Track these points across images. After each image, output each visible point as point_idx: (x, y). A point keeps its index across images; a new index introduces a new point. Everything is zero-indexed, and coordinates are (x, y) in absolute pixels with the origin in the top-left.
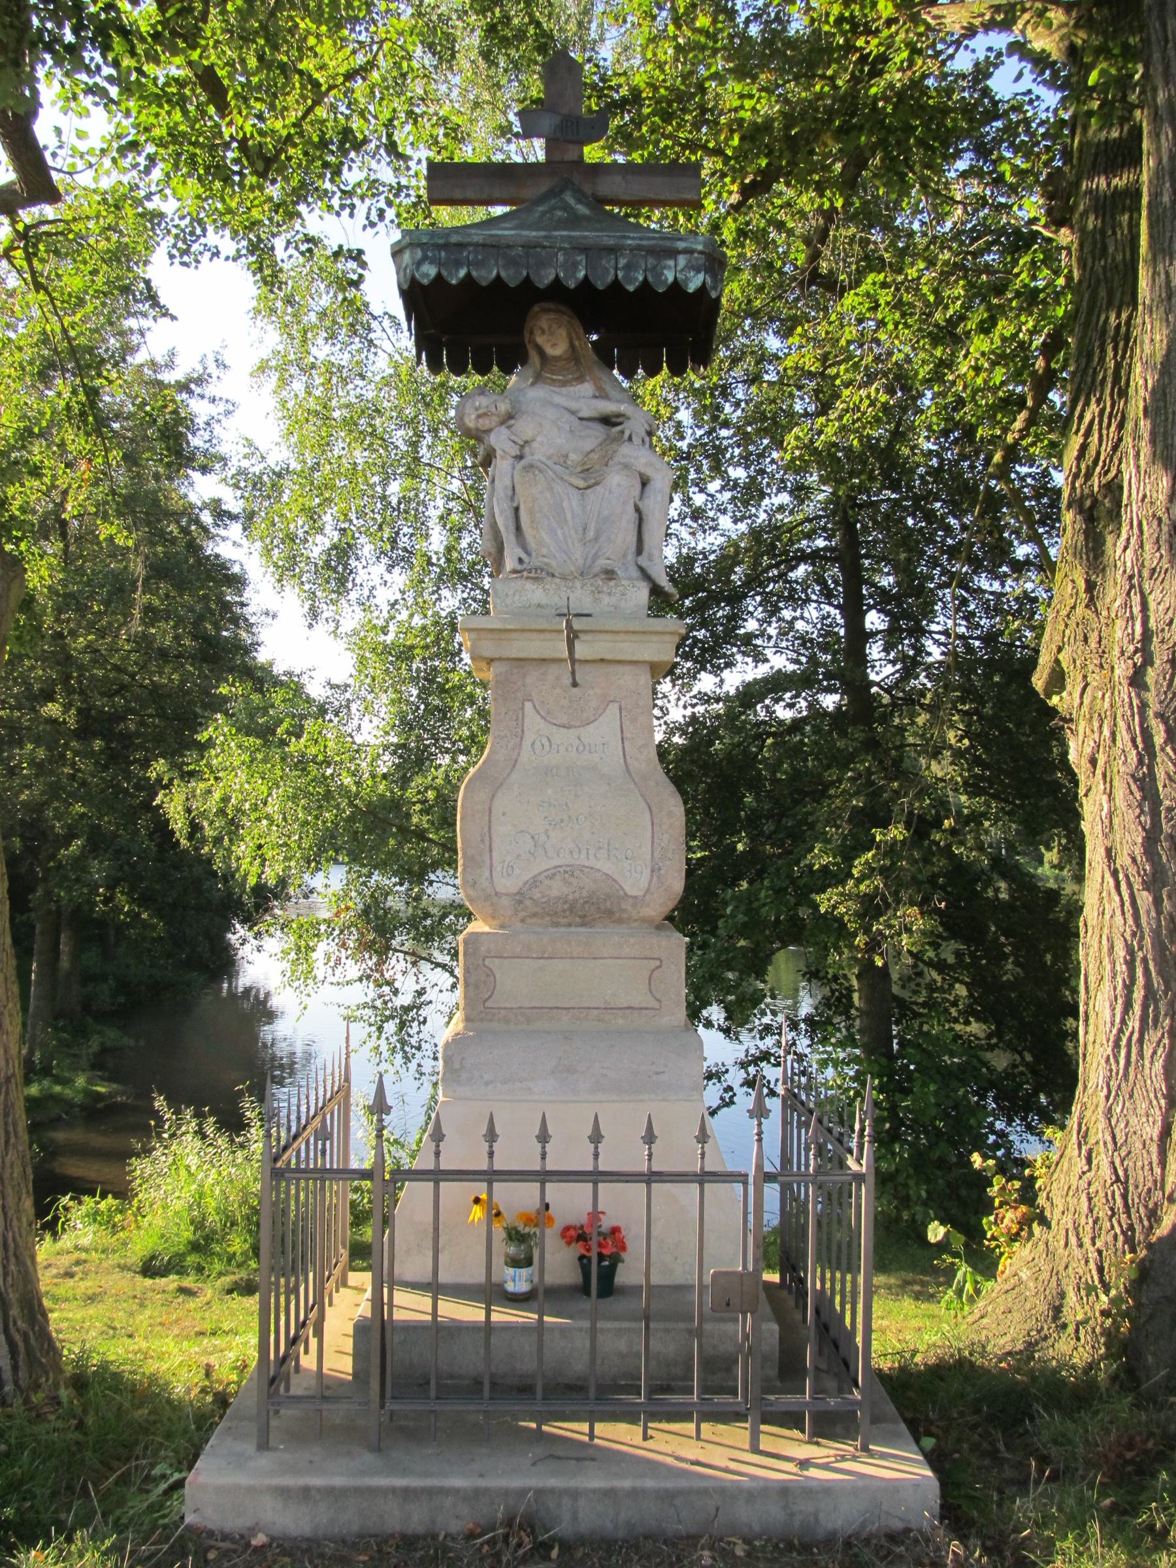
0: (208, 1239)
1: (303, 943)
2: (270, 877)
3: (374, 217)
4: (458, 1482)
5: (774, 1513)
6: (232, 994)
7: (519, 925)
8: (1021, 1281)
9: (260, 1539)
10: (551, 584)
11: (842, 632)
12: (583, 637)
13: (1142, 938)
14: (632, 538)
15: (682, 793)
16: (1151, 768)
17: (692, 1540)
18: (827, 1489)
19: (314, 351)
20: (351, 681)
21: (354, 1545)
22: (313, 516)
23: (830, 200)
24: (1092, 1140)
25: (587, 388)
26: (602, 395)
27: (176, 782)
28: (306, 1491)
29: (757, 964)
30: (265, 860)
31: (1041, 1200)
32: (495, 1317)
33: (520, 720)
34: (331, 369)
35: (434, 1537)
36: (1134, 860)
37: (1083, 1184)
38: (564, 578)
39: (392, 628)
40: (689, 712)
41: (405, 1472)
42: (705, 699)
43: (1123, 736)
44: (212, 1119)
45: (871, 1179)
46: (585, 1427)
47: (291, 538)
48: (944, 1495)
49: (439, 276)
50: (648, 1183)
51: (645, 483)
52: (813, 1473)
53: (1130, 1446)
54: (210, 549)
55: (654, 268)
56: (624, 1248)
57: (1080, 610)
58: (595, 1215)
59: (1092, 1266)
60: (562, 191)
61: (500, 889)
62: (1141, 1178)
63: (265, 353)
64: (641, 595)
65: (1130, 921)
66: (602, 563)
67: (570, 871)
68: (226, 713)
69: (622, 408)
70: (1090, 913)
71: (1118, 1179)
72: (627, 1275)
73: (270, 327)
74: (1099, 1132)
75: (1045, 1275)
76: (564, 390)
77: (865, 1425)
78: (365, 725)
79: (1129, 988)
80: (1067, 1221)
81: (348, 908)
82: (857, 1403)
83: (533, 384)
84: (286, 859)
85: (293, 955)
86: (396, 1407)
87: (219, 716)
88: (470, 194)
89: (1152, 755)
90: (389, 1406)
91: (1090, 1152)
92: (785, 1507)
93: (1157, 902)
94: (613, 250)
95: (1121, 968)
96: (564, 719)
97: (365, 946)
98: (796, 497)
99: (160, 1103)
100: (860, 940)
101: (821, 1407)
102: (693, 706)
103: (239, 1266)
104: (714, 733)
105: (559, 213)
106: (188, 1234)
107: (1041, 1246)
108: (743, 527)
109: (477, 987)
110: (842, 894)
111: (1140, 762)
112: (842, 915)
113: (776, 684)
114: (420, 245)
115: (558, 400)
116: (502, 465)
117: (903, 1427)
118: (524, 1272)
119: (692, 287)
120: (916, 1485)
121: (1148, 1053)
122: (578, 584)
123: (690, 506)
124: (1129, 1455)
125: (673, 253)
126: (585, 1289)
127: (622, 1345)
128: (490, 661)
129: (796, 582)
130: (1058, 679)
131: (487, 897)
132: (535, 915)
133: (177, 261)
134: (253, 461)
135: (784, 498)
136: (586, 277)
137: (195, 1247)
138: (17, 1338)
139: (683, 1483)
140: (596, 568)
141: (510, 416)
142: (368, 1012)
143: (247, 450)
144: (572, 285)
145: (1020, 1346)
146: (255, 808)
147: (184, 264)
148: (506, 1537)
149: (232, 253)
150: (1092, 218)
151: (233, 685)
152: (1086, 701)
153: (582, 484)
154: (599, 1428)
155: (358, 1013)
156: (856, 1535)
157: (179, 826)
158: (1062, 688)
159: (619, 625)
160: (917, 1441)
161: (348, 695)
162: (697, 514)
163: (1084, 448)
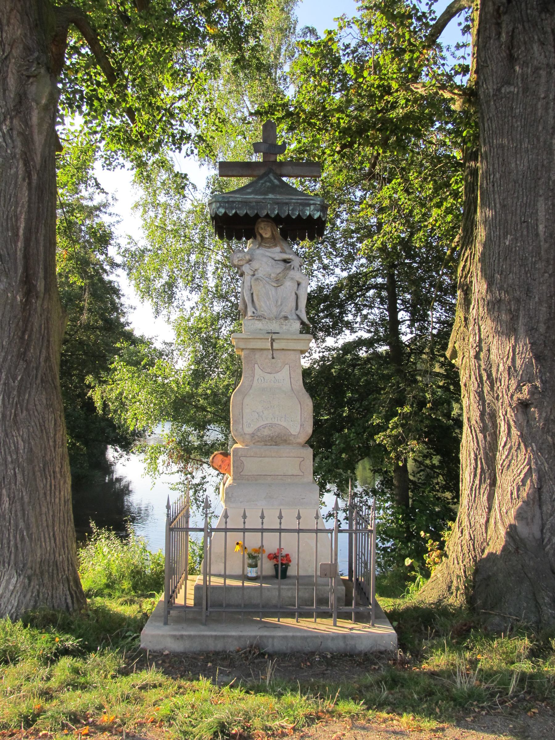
0: (113, 583)
1: (153, 456)
2: (140, 426)
3: (189, 152)
4: (234, 633)
5: (341, 645)
6: (111, 480)
7: (252, 445)
8: (437, 578)
9: (166, 652)
10: (264, 321)
11: (388, 318)
12: (276, 341)
13: (480, 451)
14: (294, 304)
15: (312, 396)
16: (482, 388)
17: (313, 653)
18: (359, 636)
19: (159, 198)
20: (174, 342)
21: (198, 654)
22: (159, 271)
23: (377, 150)
24: (463, 525)
25: (278, 249)
26: (283, 252)
27: (97, 385)
28: (182, 636)
29: (351, 466)
30: (137, 419)
31: (445, 548)
32: (245, 584)
33: (253, 371)
34: (166, 206)
35: (226, 652)
36: (477, 422)
37: (460, 541)
38: (269, 319)
39: (192, 320)
40: (321, 354)
41: (215, 631)
42: (329, 349)
43: (473, 377)
44: (114, 532)
45: (375, 532)
46: (277, 619)
47: (147, 279)
48: (399, 640)
49: (225, 213)
50: (298, 533)
51: (299, 284)
52: (354, 631)
53: (465, 625)
54: (106, 278)
55: (302, 210)
56: (290, 561)
57: (462, 328)
58: (280, 549)
59: (462, 571)
60: (269, 174)
61: (246, 432)
62: (479, 538)
63: (137, 199)
64: (297, 326)
65: (476, 444)
66: (283, 314)
67: (272, 426)
68: (119, 355)
69: (291, 257)
70: (464, 441)
71: (471, 539)
72: (292, 571)
73: (140, 188)
74: (465, 523)
75: (446, 575)
76: (269, 250)
77: (373, 617)
78: (180, 361)
79: (475, 469)
80: (454, 555)
81: (173, 441)
82: (370, 609)
83: (258, 248)
84: (147, 419)
85: (149, 461)
86: (211, 610)
87: (116, 356)
88: (234, 173)
89: (483, 385)
90: (209, 609)
91: (462, 529)
92: (345, 642)
93: (485, 437)
94: (287, 204)
95: (473, 461)
96: (269, 371)
97: (181, 457)
98: (369, 260)
99: (92, 524)
100: (392, 455)
101: (358, 610)
102: (323, 352)
103: (127, 594)
104: (331, 366)
105: (268, 184)
106: (104, 581)
107: (445, 565)
108: (345, 274)
109: (237, 467)
110: (384, 435)
111: (479, 386)
112: (385, 444)
113: (360, 343)
114: (218, 202)
115: (268, 254)
116: (247, 278)
117: (387, 620)
118: (255, 569)
119: (316, 217)
120: (389, 635)
121: (482, 493)
122: (274, 321)
123: (322, 264)
124: (464, 628)
125: (309, 205)
126: (276, 577)
127: (289, 594)
128: (243, 349)
129: (370, 297)
130: (454, 354)
131: (241, 435)
132: (258, 441)
133: (105, 168)
134: (132, 245)
135: (363, 261)
136: (278, 213)
137: (108, 586)
138: (73, 592)
139: (309, 634)
140: (281, 316)
141: (250, 261)
142: (181, 486)
143: (129, 241)
144: (273, 216)
145: (436, 601)
146: (134, 397)
147: (108, 169)
148: (250, 652)
149: (130, 167)
150: (470, 178)
151: (122, 343)
152: (464, 362)
153: (276, 285)
154: (281, 620)
155: (177, 487)
156: (369, 652)
157: (98, 404)
158: (456, 357)
159: (289, 337)
160: (392, 624)
161: (172, 348)
162: (325, 267)
163: (465, 266)
